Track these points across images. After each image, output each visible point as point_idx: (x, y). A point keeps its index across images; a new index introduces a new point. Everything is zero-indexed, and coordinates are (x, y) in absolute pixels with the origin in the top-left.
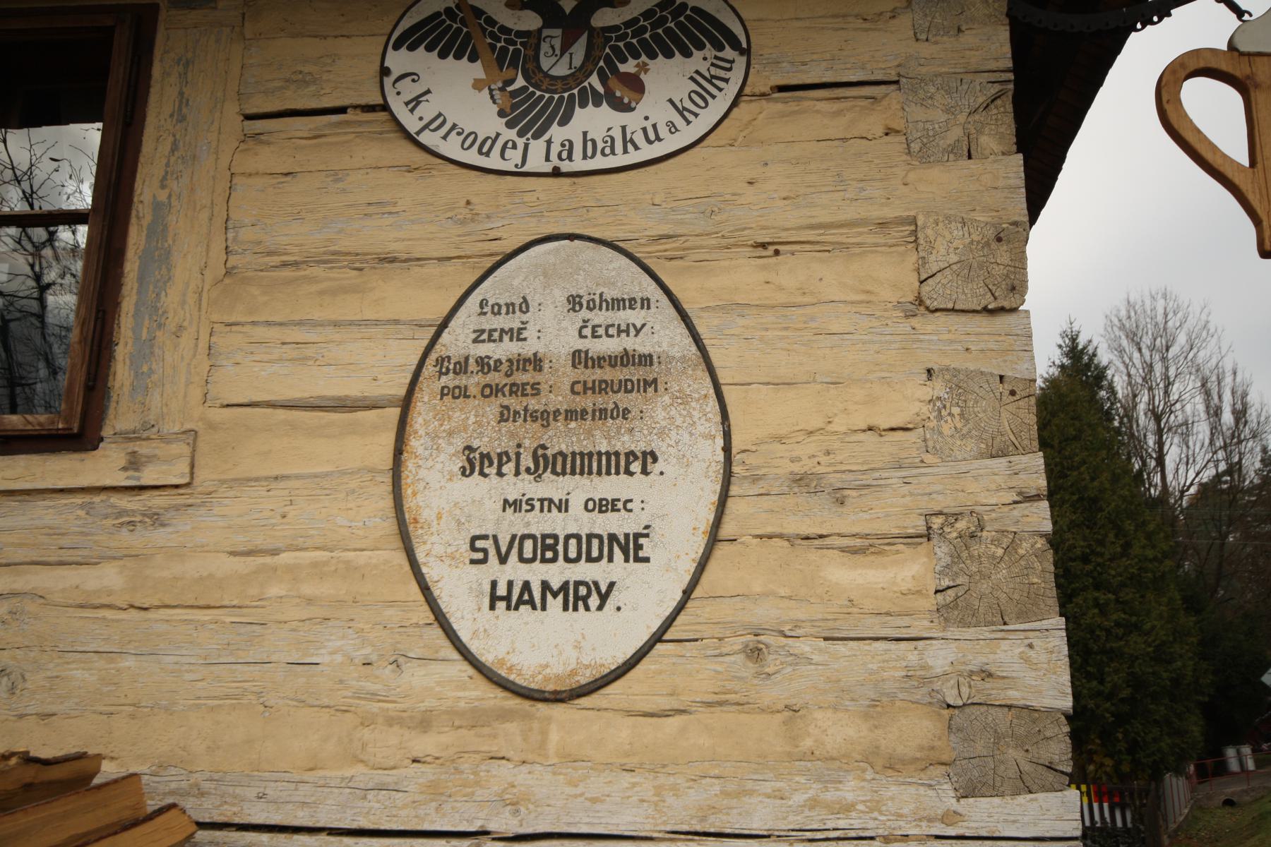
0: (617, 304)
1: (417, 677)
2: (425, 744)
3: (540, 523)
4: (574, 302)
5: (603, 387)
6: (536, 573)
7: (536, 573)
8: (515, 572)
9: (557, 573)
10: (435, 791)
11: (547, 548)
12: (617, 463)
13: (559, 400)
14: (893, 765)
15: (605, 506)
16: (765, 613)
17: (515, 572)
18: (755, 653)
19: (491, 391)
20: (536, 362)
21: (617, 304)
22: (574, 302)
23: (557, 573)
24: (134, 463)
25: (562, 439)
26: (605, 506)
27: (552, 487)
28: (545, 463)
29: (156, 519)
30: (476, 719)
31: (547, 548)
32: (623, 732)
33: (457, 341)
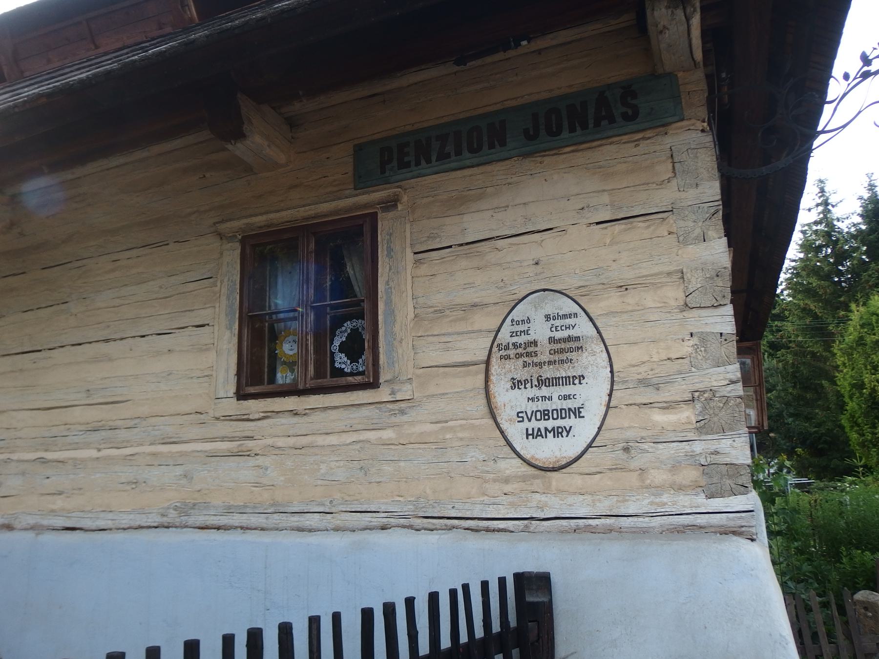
0: (565, 316)
1: (502, 465)
2: (508, 488)
3: (541, 406)
4: (548, 317)
5: (562, 351)
6: (542, 424)
7: (542, 424)
8: (534, 424)
9: (550, 424)
10: (512, 504)
11: (546, 415)
12: (568, 380)
13: (545, 357)
14: (680, 488)
15: (566, 397)
16: (630, 434)
17: (534, 424)
18: (626, 450)
19: (519, 356)
20: (535, 343)
21: (565, 316)
22: (548, 317)
23: (550, 424)
24: (393, 393)
25: (548, 372)
26: (566, 397)
27: (545, 391)
28: (542, 382)
29: (402, 412)
30: (524, 479)
31: (546, 415)
32: (578, 481)
33: (504, 336)
